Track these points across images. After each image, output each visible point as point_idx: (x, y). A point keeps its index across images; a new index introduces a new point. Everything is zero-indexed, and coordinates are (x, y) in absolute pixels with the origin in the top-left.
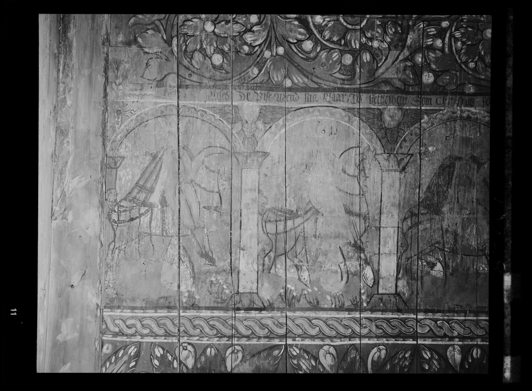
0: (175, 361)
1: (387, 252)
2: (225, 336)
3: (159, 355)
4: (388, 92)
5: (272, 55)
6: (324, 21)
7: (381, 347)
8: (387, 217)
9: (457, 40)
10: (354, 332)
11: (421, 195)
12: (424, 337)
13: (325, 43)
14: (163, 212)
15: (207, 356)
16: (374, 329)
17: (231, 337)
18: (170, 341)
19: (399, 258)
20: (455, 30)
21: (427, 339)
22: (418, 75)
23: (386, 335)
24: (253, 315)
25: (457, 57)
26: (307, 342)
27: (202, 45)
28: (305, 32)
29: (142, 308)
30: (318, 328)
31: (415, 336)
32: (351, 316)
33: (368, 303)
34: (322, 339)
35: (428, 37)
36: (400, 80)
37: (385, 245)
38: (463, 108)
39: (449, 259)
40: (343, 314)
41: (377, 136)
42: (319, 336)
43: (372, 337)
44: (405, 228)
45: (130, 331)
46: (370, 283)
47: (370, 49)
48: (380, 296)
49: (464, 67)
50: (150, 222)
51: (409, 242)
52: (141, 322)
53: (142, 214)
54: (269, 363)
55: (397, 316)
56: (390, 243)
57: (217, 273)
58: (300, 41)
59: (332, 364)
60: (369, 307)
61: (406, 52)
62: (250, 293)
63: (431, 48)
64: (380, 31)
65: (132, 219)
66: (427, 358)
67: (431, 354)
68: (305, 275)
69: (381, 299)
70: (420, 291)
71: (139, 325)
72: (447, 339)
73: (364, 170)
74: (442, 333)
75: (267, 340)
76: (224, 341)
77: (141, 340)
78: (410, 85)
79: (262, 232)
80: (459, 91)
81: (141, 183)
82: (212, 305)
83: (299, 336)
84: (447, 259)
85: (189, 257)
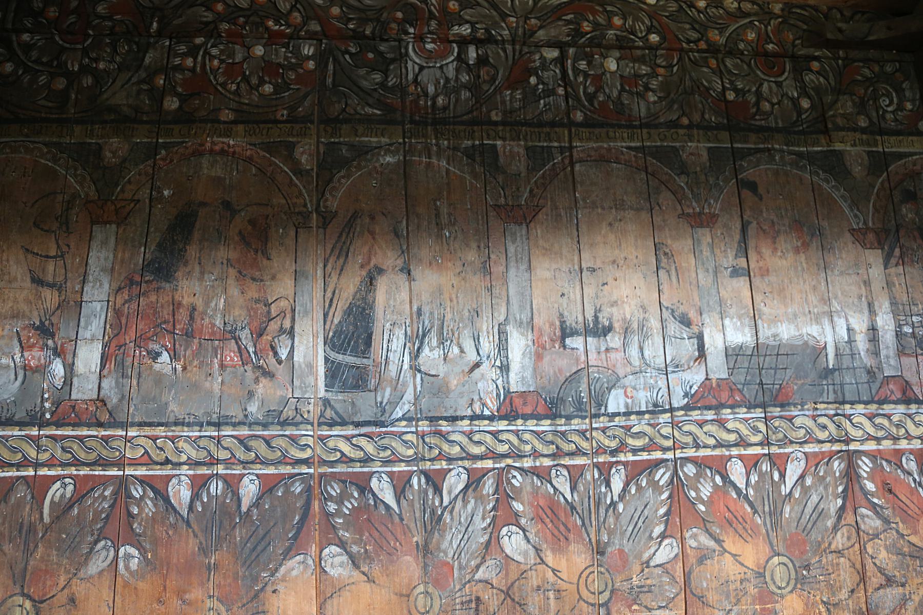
6: (32, 39)
7: (67, 480)
9: (212, 57)
11: (147, 256)
12: (134, 463)
16: (59, 453)
19: (104, 346)
20: (212, 47)
21: (140, 467)
22: (158, 97)
23: (76, 462)
25: (212, 78)
31: (120, 464)
32: (23, 433)
33: (52, 414)
35: (177, 55)
37: (86, 328)
38: (215, 139)
39: (181, 346)
40: (11, 430)
43: (54, 465)
44: (119, 301)
46: (59, 383)
47: (95, 73)
48: (73, 403)
55: (95, 433)
56: (94, 324)
60: (55, 419)
61: (143, 74)
63: (179, 68)
64: (109, 51)
66: (138, 496)
67: (144, 491)
69: (74, 407)
73: (67, 223)
74: (161, 457)
84: (177, 346)
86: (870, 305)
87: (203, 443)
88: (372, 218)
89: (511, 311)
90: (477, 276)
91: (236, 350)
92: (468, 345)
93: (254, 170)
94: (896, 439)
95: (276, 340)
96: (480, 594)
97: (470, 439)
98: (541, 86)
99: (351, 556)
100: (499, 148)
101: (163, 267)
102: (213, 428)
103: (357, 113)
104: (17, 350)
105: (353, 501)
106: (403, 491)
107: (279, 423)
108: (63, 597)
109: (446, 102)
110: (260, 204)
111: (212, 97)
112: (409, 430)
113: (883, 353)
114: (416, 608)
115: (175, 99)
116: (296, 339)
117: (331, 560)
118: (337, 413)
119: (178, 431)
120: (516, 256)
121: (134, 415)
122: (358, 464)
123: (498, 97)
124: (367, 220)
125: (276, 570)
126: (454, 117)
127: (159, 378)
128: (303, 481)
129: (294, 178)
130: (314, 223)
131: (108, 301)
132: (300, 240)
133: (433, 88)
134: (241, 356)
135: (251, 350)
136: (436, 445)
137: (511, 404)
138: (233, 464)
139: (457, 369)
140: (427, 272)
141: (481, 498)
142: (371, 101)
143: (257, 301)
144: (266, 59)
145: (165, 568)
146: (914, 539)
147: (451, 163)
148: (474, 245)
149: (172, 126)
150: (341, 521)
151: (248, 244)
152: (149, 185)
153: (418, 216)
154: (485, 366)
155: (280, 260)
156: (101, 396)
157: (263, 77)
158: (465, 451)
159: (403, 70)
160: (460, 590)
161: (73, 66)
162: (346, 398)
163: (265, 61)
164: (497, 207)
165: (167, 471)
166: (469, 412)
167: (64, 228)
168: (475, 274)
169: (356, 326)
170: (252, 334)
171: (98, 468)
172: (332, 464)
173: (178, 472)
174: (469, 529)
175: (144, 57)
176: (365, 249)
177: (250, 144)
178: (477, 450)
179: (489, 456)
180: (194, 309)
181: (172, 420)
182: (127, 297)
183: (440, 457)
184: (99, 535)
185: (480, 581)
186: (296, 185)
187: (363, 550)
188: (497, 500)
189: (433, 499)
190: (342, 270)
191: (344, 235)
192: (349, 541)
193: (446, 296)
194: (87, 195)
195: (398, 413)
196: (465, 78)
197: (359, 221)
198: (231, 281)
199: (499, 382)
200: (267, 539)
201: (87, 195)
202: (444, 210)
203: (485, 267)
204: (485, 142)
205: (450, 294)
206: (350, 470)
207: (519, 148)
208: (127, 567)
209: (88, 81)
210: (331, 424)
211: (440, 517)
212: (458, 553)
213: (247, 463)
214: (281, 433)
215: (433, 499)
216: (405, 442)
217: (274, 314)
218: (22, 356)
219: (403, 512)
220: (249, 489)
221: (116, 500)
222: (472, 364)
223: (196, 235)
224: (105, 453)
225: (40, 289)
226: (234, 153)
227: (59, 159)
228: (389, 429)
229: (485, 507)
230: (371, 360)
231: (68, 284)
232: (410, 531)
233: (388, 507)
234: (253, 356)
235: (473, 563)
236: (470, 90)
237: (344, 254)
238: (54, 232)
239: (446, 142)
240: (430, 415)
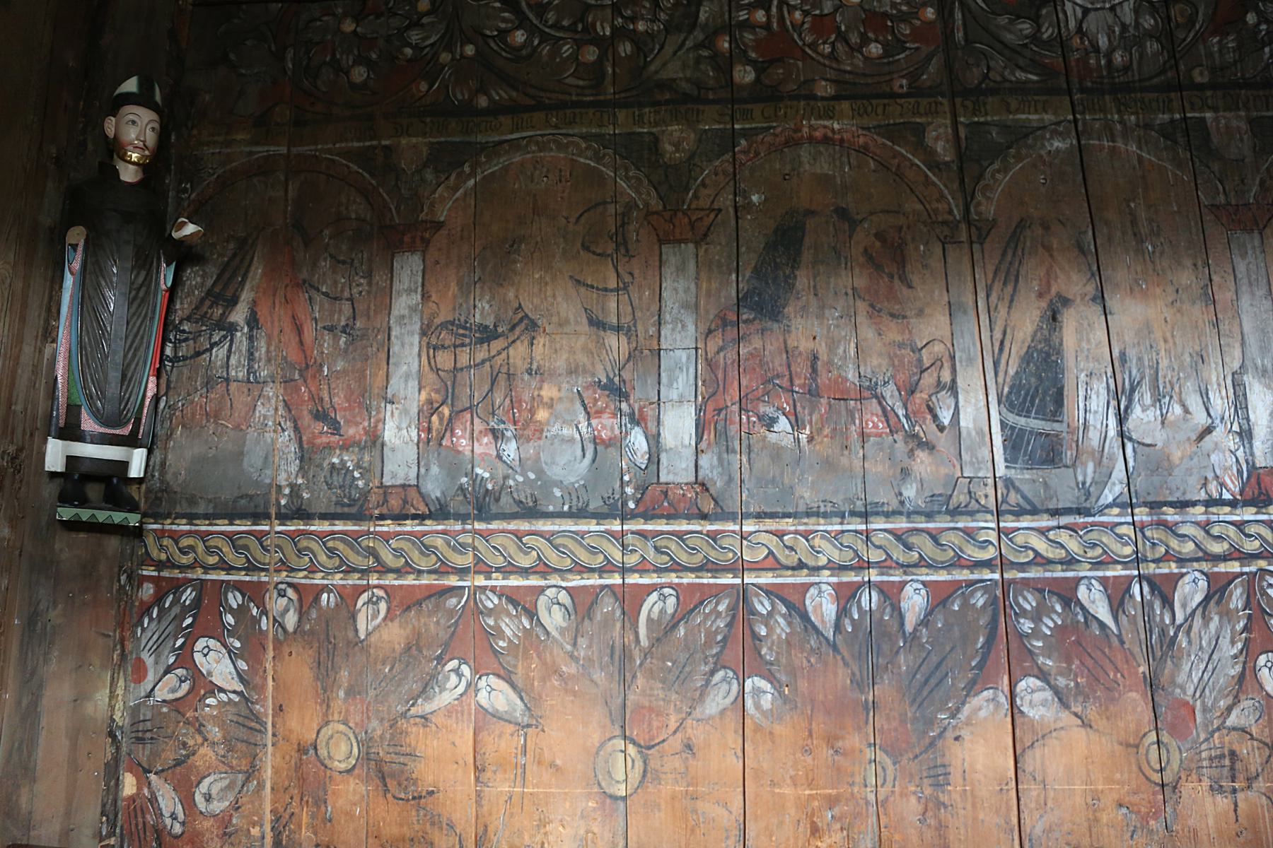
0: (264, 618)
1: (675, 397)
2: (355, 570)
3: (235, 606)
4: (667, 102)
5: (452, 59)
7: (667, 591)
8: (673, 330)
10: (609, 561)
11: (741, 286)
12: (757, 568)
13: (547, 30)
14: (251, 338)
15: (321, 608)
16: (651, 555)
18: (255, 579)
19: (698, 410)
21: (764, 573)
22: (724, 65)
23: (675, 566)
24: (408, 529)
26: (514, 581)
27: (334, 55)
28: (513, 17)
29: (206, 516)
30: (534, 553)
31: (739, 567)
32: (602, 528)
33: (637, 502)
34: (544, 575)
36: (688, 80)
37: (670, 385)
38: (813, 122)
40: (587, 524)
41: (650, 181)
42: (538, 569)
44: (712, 346)
45: (185, 560)
46: (642, 461)
47: (633, 37)
49: (810, 52)
50: (228, 358)
51: (720, 376)
52: (204, 542)
53: (216, 344)
54: (438, 623)
55: (698, 528)
56: (680, 380)
57: (345, 448)
58: (503, 33)
59: (564, 625)
61: (699, 35)
62: (403, 486)
63: (747, 25)
65: (198, 354)
66: (765, 612)
67: (773, 605)
68: (510, 450)
69: (666, 494)
70: (746, 476)
71: (201, 548)
72: (805, 571)
73: (625, 243)
74: (792, 560)
75: (434, 576)
76: (354, 580)
77: (203, 577)
78: (708, 89)
79: (427, 368)
80: (803, 92)
81: (217, 290)
82: (332, 510)
83: (498, 570)
84: (799, 409)
85: (295, 421)
87: (847, 539)
88: (1046, 227)
89: (1248, 355)
90: (1198, 306)
91: (880, 412)
92: (1194, 403)
93: (872, 165)
95: (934, 398)
96: (1236, 747)
97: (1207, 532)
98: (1264, 27)
99: (1057, 692)
100: (1209, 122)
101: (762, 301)
102: (859, 520)
103: (1005, 80)
104: (582, 416)
105: (1055, 617)
106: (1122, 603)
107: (948, 512)
108: (676, 743)
109: (1127, 58)
110: (888, 212)
111: (800, 64)
112: (1123, 520)
114: (1148, 763)
115: (748, 68)
116: (960, 397)
117: (1028, 697)
118: (1024, 497)
119: (811, 524)
120: (1249, 277)
121: (748, 503)
122: (1059, 567)
123: (1201, 47)
124: (1040, 231)
125: (958, 710)
126: (1140, 81)
127: (777, 453)
128: (986, 590)
129: (930, 174)
130: (964, 237)
131: (696, 349)
132: (949, 260)
133: (1106, 39)
134: (887, 421)
135: (901, 412)
136: (1161, 541)
137: (1259, 484)
138: (890, 568)
139: (1181, 436)
140: (1127, 301)
141: (1227, 614)
142: (1021, 62)
143: (901, 345)
144: (867, 7)
145: (809, 707)
147: (1144, 148)
148: (1188, 263)
149: (749, 106)
150: (1040, 644)
151: (878, 267)
152: (730, 188)
153: (1107, 223)
154: (1219, 432)
155: (927, 290)
156: (700, 478)
157: (865, 33)
158: (1201, 549)
159: (1061, 15)
160: (1207, 740)
161: (603, 28)
162: (1035, 477)
163: (864, 10)
164: (1214, 207)
165: (802, 578)
166: (1203, 495)
167: (623, 250)
168: (1194, 303)
169: (1040, 378)
170: (899, 390)
171: (705, 574)
172: (1022, 567)
173: (816, 579)
174: (1215, 656)
175: (698, 12)
176: (1042, 272)
177: (863, 128)
178: (1217, 548)
179: (1234, 556)
180: (815, 358)
181: (802, 508)
182: (721, 343)
183: (1167, 557)
184: (715, 663)
185: (1234, 729)
186: (934, 184)
187: (1072, 684)
188: (1250, 617)
189: (1162, 615)
190: (1011, 301)
191: (1010, 253)
192: (1053, 672)
193: (1158, 335)
194: (647, 204)
195: (1108, 497)
196: (1148, 22)
197: (1028, 232)
198: (862, 319)
199: (1240, 454)
200: (943, 669)
201: (647, 204)
202: (1142, 214)
203: (1206, 294)
204: (1189, 115)
205: (1164, 333)
206: (1048, 575)
207: (1238, 120)
208: (758, 706)
209: (625, 48)
210: (1018, 513)
211: (1173, 640)
212: (1201, 688)
213: (908, 566)
214: (952, 525)
215: (1162, 615)
216: (1120, 536)
217: (927, 363)
218: (589, 424)
219: (1123, 632)
220: (914, 601)
221: (734, 617)
222: (1200, 429)
223: (807, 256)
224: (713, 556)
225: (602, 333)
226: (842, 140)
227: (604, 156)
228: (1097, 519)
229: (1234, 627)
230: (1065, 425)
231: (640, 327)
232: (1135, 658)
233: (1102, 625)
234: (904, 420)
235: (1222, 703)
236: (1158, 40)
237: (1013, 278)
238: (611, 256)
239: (1133, 118)
240: (1150, 499)
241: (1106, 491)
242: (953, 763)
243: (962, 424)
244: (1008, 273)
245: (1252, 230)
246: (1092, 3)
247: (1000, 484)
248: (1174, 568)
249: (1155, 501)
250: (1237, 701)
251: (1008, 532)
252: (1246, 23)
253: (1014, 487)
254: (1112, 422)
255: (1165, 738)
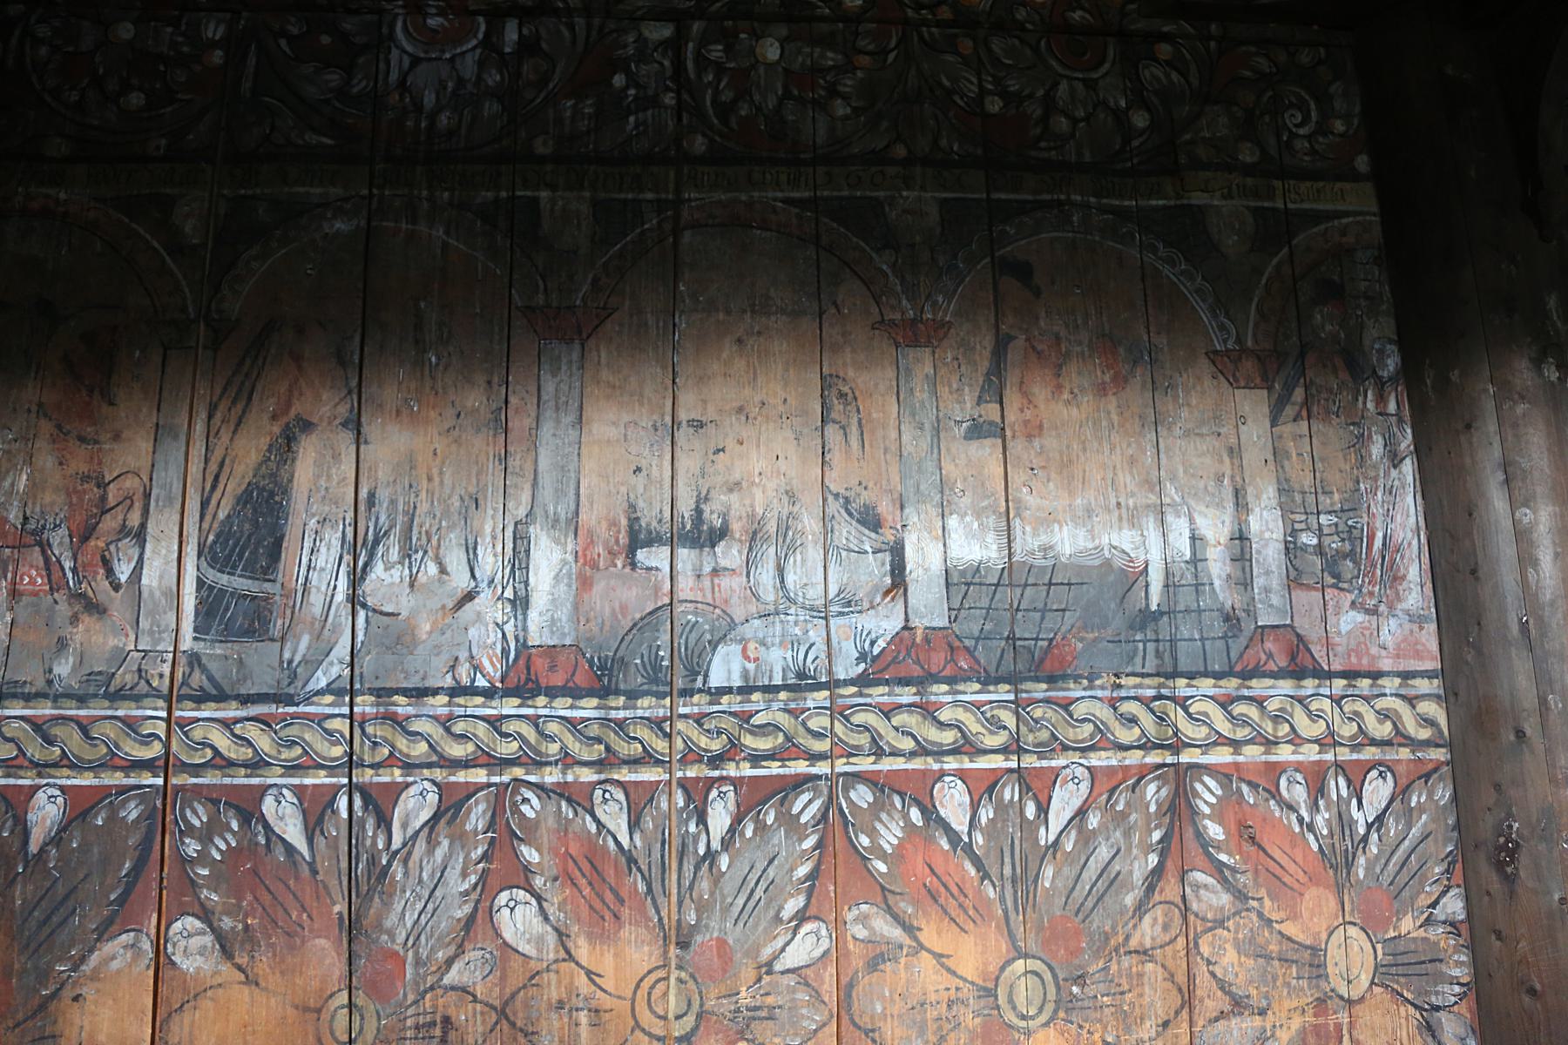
17: (716, 760)
86: (1238, 494)
89: (539, 499)
91: (41, 563)
92: (456, 560)
94: (1270, 743)
95: (112, 548)
96: (452, 1012)
97: (448, 730)
98: (632, 92)
105: (229, 837)
106: (320, 821)
112: (337, 711)
113: (1259, 582)
114: (332, 1034)
116: (148, 547)
117: (183, 943)
118: (211, 679)
120: (557, 398)
122: (243, 771)
128: (142, 799)
133: (433, 96)
134: (49, 576)
136: (386, 740)
137: (528, 669)
138: (21, 767)
139: (435, 604)
143: (86, 478)
146: (1290, 929)
148: (481, 379)
150: (206, 872)
154: (484, 598)
159: (382, 66)
160: (416, 1002)
166: (448, 681)
170: (71, 537)
172: (196, 769)
174: (438, 893)
178: (457, 751)
179: (480, 761)
183: (391, 761)
185: (453, 988)
187: (240, 926)
188: (492, 842)
189: (375, 837)
190: (238, 424)
191: (248, 362)
193: (422, 473)
200: (70, 903)
204: (518, 193)
206: (227, 781)
210: (200, 699)
212: (416, 934)
213: (46, 766)
214: (109, 713)
215: (375, 837)
216: (329, 733)
217: (112, 501)
222: (459, 595)
228: (302, 709)
230: (278, 585)
232: (329, 894)
233: (290, 849)
234: (70, 575)
235: (440, 954)
237: (245, 395)
241: (319, 672)
242: (67, 1032)
243: (144, 581)
244: (240, 390)
245: (572, 340)
246: (426, 52)
247: (182, 660)
248: (397, 775)
249: (381, 689)
250: (461, 950)
251: (184, 724)
252: (611, 85)
253: (200, 664)
254: (343, 584)
255: (360, 999)
